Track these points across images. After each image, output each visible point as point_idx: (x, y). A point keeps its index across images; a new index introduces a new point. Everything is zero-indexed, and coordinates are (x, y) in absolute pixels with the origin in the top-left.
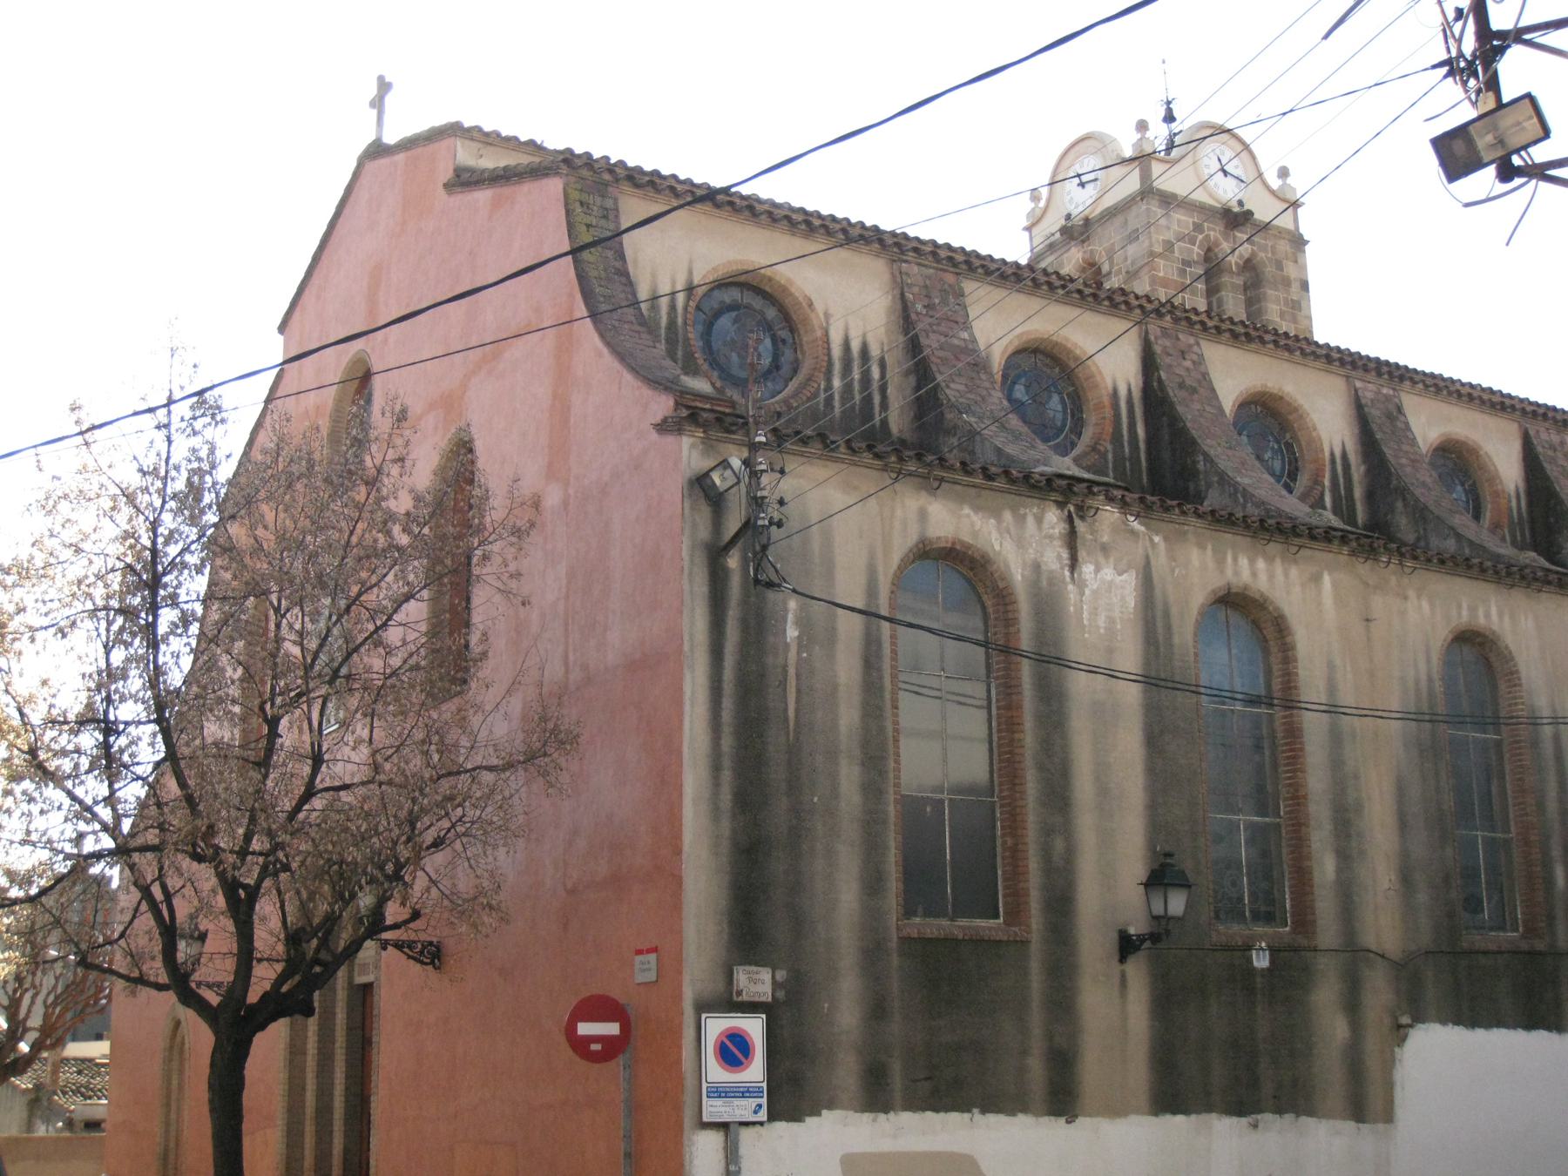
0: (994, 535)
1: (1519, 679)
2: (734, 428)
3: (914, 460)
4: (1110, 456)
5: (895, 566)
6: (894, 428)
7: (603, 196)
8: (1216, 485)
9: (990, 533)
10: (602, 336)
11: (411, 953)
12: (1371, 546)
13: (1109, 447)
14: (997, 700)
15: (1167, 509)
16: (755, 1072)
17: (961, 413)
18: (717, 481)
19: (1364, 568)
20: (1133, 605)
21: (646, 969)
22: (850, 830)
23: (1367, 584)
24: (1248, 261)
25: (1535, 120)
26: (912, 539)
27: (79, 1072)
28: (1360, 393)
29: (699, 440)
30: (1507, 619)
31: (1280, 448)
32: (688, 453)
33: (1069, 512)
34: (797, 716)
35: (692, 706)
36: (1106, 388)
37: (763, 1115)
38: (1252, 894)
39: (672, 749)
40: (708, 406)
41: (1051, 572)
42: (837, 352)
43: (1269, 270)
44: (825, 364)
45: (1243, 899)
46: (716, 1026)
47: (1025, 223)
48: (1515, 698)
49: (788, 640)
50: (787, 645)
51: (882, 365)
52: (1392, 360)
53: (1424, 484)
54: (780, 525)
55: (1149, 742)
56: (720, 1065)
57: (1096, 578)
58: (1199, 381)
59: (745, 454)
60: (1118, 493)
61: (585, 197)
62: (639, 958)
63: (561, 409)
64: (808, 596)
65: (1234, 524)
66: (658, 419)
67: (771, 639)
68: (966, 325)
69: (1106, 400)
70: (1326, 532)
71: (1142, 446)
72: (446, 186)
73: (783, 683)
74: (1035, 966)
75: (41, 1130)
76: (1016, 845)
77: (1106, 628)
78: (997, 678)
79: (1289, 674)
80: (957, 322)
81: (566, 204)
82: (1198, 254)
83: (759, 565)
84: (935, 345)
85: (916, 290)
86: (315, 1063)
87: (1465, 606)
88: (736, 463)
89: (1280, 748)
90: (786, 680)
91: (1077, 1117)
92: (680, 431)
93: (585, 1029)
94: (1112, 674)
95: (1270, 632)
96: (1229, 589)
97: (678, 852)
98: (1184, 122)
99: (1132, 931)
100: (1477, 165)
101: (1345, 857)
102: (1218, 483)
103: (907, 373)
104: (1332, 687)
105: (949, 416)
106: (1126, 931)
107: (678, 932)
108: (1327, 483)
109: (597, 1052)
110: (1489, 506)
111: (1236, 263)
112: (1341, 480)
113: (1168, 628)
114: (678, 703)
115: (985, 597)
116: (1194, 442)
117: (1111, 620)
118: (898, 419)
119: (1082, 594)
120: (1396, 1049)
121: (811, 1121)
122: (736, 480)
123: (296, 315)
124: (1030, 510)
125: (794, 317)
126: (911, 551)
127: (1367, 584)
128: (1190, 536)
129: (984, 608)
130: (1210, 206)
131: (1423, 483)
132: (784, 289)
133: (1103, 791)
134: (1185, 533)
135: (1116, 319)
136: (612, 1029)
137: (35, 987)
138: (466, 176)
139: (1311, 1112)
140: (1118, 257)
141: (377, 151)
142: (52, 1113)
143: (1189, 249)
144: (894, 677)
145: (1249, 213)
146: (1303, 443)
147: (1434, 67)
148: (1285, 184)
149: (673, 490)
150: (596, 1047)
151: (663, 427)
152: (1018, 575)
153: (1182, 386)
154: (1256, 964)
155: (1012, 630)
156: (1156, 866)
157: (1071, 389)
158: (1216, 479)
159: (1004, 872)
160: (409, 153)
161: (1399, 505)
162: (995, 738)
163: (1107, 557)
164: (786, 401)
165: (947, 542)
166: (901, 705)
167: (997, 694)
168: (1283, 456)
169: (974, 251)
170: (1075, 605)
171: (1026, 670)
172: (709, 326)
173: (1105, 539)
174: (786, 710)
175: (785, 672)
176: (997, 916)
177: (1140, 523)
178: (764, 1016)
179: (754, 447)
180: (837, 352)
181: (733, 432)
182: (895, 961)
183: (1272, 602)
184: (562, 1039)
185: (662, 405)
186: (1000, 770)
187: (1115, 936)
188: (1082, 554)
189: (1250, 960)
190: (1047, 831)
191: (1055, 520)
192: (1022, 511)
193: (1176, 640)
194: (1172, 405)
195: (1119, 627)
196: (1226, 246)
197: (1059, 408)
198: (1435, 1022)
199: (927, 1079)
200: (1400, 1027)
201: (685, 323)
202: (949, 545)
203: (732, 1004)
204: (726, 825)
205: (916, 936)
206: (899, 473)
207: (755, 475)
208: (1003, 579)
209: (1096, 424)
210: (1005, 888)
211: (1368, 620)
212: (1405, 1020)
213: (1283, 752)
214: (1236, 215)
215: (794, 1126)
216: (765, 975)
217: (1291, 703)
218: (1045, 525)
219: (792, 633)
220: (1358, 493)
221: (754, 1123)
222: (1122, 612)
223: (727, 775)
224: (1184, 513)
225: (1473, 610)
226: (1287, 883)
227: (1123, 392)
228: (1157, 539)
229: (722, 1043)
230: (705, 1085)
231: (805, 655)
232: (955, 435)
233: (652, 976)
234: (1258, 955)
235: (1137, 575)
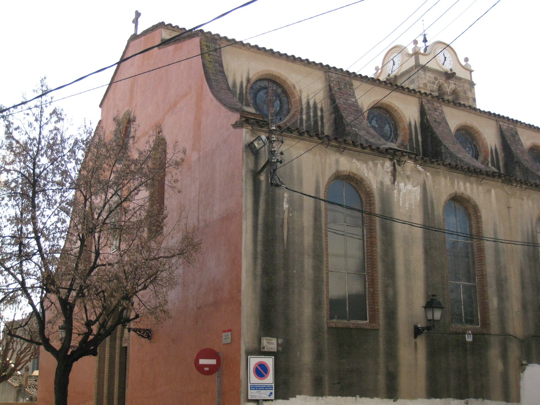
0: (365, 170)
3: (334, 140)
5: (326, 181)
6: (326, 133)
7: (215, 44)
9: (364, 170)
10: (213, 93)
12: (510, 179)
13: (408, 144)
15: (432, 163)
16: (270, 379)
17: (352, 127)
18: (256, 145)
19: (507, 188)
21: (226, 338)
22: (308, 284)
23: (508, 194)
24: (454, 91)
26: (334, 170)
27: (36, 381)
28: (501, 127)
29: (249, 130)
31: (472, 146)
34: (287, 239)
35: (246, 234)
36: (407, 122)
37: (272, 397)
38: (465, 313)
39: (239, 252)
40: (253, 117)
41: (387, 185)
42: (304, 106)
43: (461, 94)
45: (462, 315)
46: (254, 361)
49: (284, 209)
50: (284, 211)
51: (322, 110)
53: (526, 160)
54: (281, 162)
56: (255, 376)
57: (405, 188)
58: (442, 120)
59: (268, 135)
60: (413, 156)
61: (208, 44)
62: (224, 334)
63: (198, 124)
64: (293, 191)
65: (458, 169)
67: (277, 208)
68: (354, 96)
70: (493, 173)
71: (420, 144)
73: (282, 226)
74: (381, 339)
75: (21, 401)
76: (374, 291)
77: (409, 208)
78: (367, 226)
79: (479, 227)
80: (350, 95)
81: (201, 46)
82: (436, 88)
83: (272, 178)
84: (342, 103)
85: (335, 83)
86: (107, 376)
88: (264, 137)
89: (476, 256)
91: (397, 399)
92: (242, 127)
93: (202, 362)
94: (411, 224)
95: (471, 211)
97: (240, 291)
99: (419, 326)
101: (502, 299)
102: (450, 157)
104: (495, 233)
105: (347, 129)
106: (417, 326)
107: (239, 323)
108: (489, 159)
109: (206, 371)
111: (450, 92)
113: (433, 208)
114: (241, 233)
115: (362, 195)
116: (440, 141)
117: (410, 204)
118: (327, 130)
119: (399, 194)
120: (521, 374)
121: (292, 400)
122: (263, 145)
123: (106, 100)
124: (379, 162)
125: (288, 92)
126: (333, 175)
127: (508, 194)
128: (441, 173)
129: (361, 199)
131: (526, 160)
132: (285, 81)
133: (408, 271)
134: (439, 172)
135: (410, 97)
136: (213, 362)
137: (13, 349)
139: (489, 398)
141: (134, 37)
142: (25, 394)
144: (326, 224)
145: (454, 73)
148: (467, 64)
149: (240, 148)
150: (206, 369)
151: (236, 125)
152: (374, 186)
153: (435, 121)
154: (467, 340)
155: (372, 207)
156: (429, 300)
157: (393, 122)
159: (369, 302)
160: (145, 36)
161: (517, 168)
162: (366, 248)
163: (409, 181)
164: (285, 123)
165: (347, 172)
166: (328, 235)
168: (473, 149)
170: (397, 199)
171: (377, 220)
172: (255, 95)
173: (408, 173)
174: (283, 236)
175: (283, 223)
176: (366, 320)
177: (422, 168)
178: (273, 357)
179: (271, 132)
180: (304, 106)
182: (326, 336)
183: (472, 200)
184: (193, 365)
185: (236, 117)
186: (368, 262)
187: (413, 328)
188: (398, 179)
190: (386, 286)
191: (389, 165)
192: (376, 162)
193: (436, 213)
194: (431, 128)
195: (414, 207)
196: (446, 85)
197: (389, 129)
198: (535, 363)
199: (338, 383)
200: (522, 365)
201: (246, 93)
202: (348, 174)
204: (259, 281)
205: (334, 326)
206: (328, 145)
207: (271, 142)
208: (369, 188)
209: (402, 136)
210: (369, 308)
211: (509, 207)
212: (524, 362)
213: (477, 258)
214: (450, 74)
215: (285, 402)
216: (274, 341)
217: (480, 238)
218: (385, 167)
219: (286, 206)
221: (269, 400)
223: (259, 261)
224: (439, 164)
226: (479, 309)
228: (428, 174)
229: (257, 368)
230: (249, 385)
232: (350, 136)
233: (229, 341)
234: (468, 337)
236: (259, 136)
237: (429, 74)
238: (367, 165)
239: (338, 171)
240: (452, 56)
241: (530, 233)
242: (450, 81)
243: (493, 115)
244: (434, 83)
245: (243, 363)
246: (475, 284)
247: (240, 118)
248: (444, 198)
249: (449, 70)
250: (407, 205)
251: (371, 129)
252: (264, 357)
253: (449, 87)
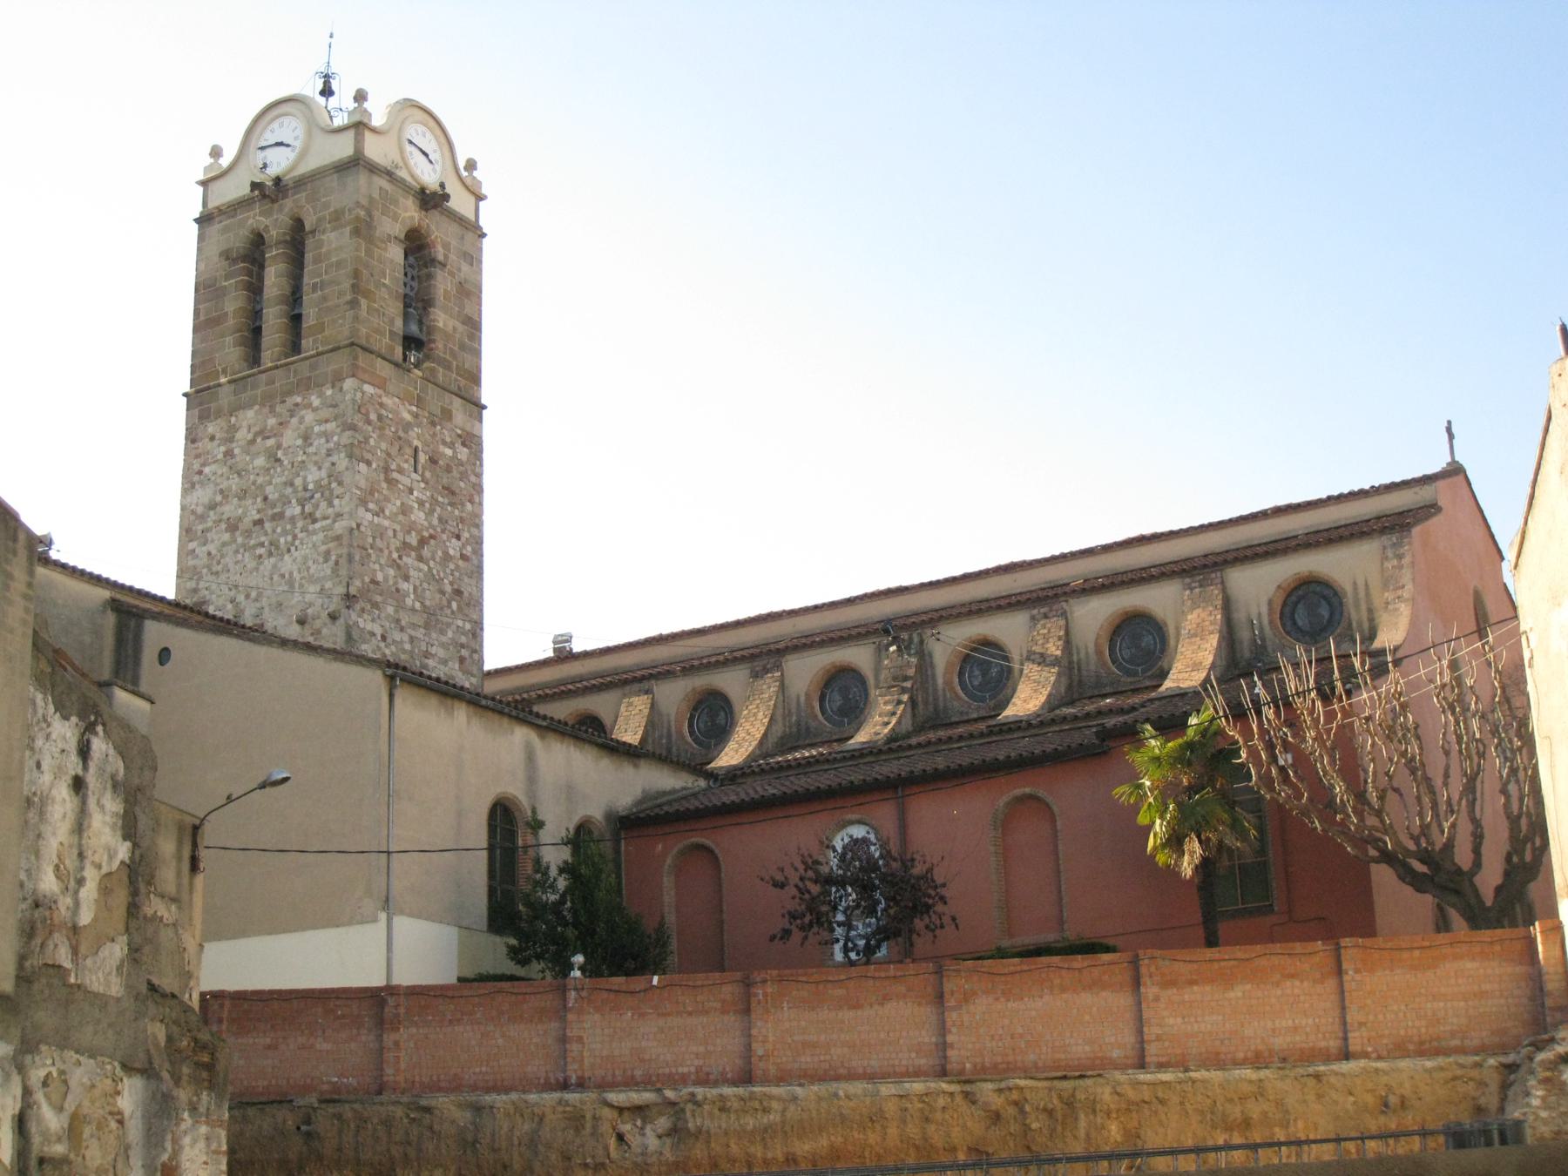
121: (1461, 462)
240: (441, 150)
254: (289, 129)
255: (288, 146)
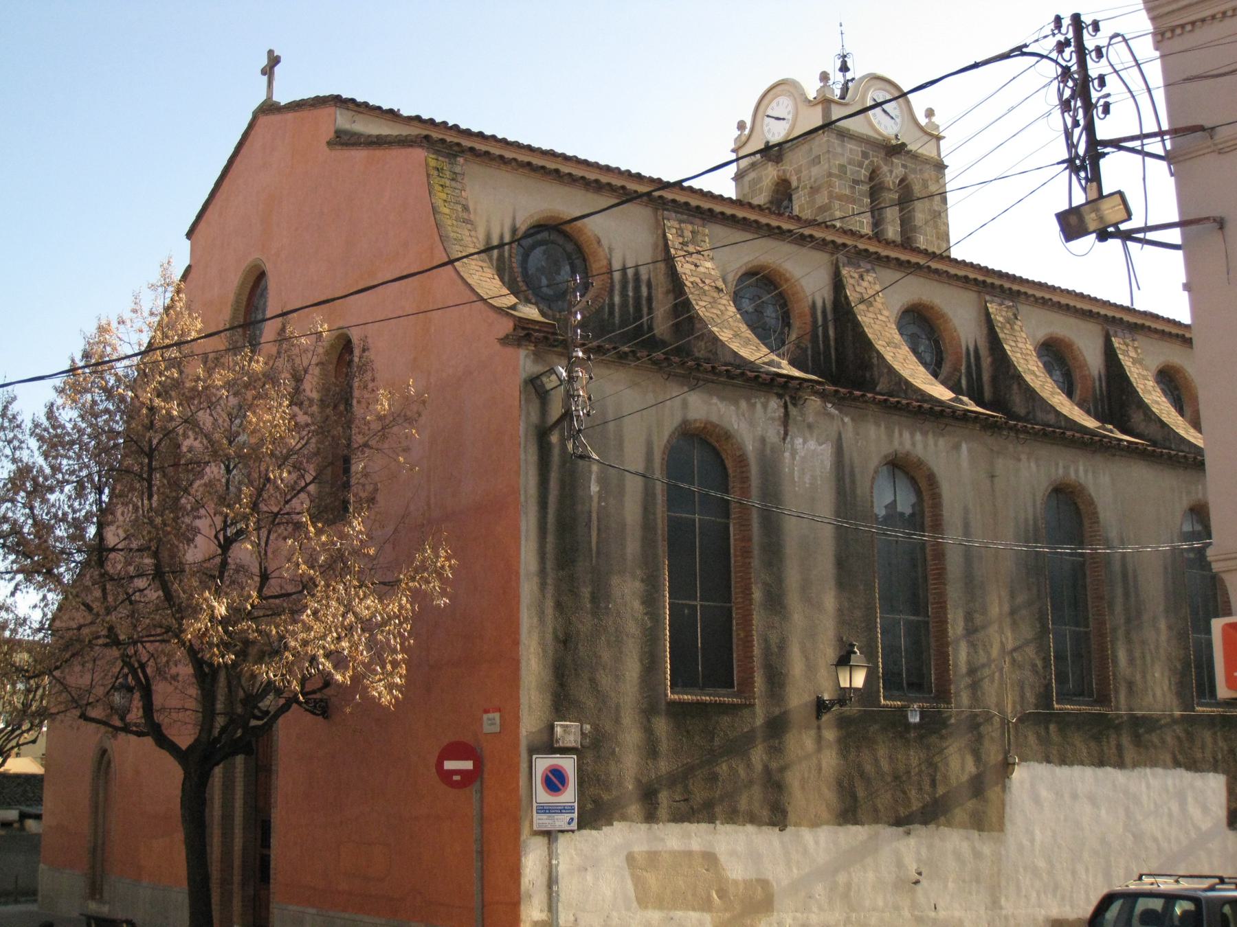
0: (734, 419)
1: (1098, 518)
2: (556, 343)
4: (809, 352)
8: (885, 375)
11: (307, 707)
13: (809, 346)
14: (734, 535)
16: (569, 795)
20: (829, 467)
25: (1122, 207)
26: (677, 420)
30: (1090, 475)
32: (524, 362)
33: (785, 400)
37: (574, 826)
38: (907, 670)
42: (617, 276)
43: (917, 189)
44: (608, 285)
46: (542, 764)
47: (732, 146)
48: (1095, 531)
50: (591, 497)
52: (1011, 273)
55: (839, 564)
56: (547, 792)
65: (900, 409)
66: (501, 335)
69: (807, 310)
71: (832, 343)
72: (329, 143)
77: (810, 484)
84: (688, 272)
87: (1061, 465)
90: (590, 521)
92: (519, 345)
93: (449, 765)
96: (896, 455)
98: (856, 71)
99: (826, 697)
100: (1085, 233)
103: (668, 292)
110: (1079, 385)
112: (974, 367)
113: (853, 482)
118: (662, 326)
119: (793, 458)
120: (1007, 780)
122: (559, 383)
123: (202, 224)
126: (676, 429)
130: (874, 138)
136: (468, 765)
138: (345, 138)
140: (805, 173)
141: (268, 108)
143: (858, 171)
146: (947, 341)
147: (1059, 163)
150: (457, 778)
151: (505, 341)
152: (750, 447)
158: (886, 371)
161: (1015, 387)
167: (734, 531)
169: (709, 192)
172: (526, 257)
174: (590, 542)
175: (590, 521)
177: (836, 409)
178: (575, 757)
180: (617, 276)
181: (555, 346)
188: (793, 430)
189: (906, 717)
191: (776, 406)
193: (859, 492)
196: (885, 169)
201: (510, 256)
203: (550, 747)
209: (798, 328)
213: (933, 570)
216: (574, 725)
218: (769, 410)
219: (594, 488)
220: (986, 377)
221: (568, 831)
222: (822, 472)
225: (1066, 468)
227: (819, 304)
228: (846, 420)
229: (547, 776)
230: (535, 805)
231: (603, 504)
232: (702, 340)
235: (832, 446)
236: (552, 369)
237: (850, 145)
238: (738, 408)
239: (687, 421)
241: (1031, 522)
242: (895, 161)
243: (973, 282)
244: (860, 165)
245: (524, 766)
246: (927, 619)
247: (514, 330)
248: (874, 462)
249: (893, 136)
250: (807, 479)
251: (741, 325)
252: (558, 756)
253: (891, 172)
254: (783, 106)
255: (784, 119)
